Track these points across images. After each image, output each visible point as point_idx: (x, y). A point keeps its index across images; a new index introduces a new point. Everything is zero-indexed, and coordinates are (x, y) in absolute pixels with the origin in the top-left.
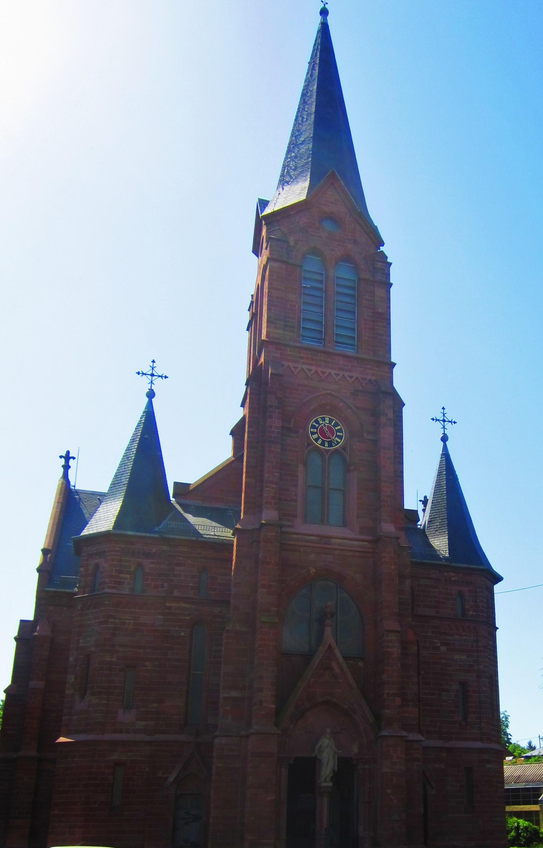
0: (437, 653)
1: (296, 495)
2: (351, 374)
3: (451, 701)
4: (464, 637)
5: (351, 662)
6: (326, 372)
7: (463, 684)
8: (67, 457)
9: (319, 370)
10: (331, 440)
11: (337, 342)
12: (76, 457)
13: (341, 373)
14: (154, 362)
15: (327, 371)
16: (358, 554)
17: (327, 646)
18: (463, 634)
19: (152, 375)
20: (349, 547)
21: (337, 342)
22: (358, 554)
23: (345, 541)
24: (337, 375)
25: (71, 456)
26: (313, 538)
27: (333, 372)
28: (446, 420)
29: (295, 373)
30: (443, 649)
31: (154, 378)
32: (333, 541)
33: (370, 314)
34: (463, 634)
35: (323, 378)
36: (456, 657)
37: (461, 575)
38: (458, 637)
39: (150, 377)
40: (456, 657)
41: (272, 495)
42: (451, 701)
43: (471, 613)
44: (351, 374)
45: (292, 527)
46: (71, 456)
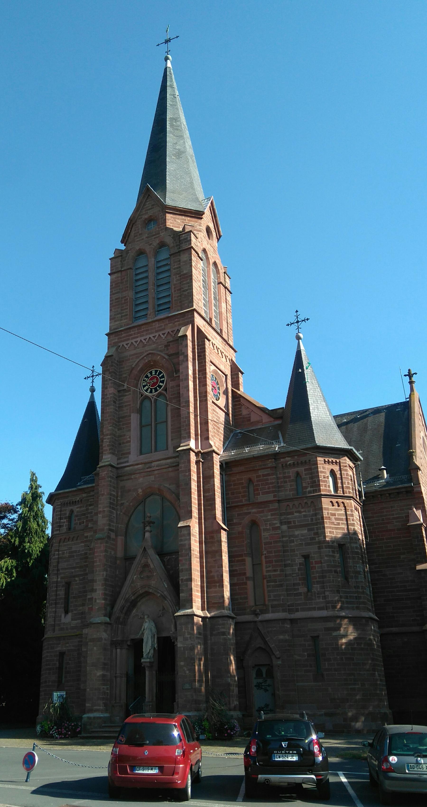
0: (277, 532)
1: (130, 437)
2: (163, 332)
3: (295, 575)
4: (304, 513)
5: (174, 556)
6: (147, 338)
7: (306, 557)
8: (410, 375)
9: (151, 336)
10: (157, 386)
11: (158, 311)
12: (403, 376)
13: (157, 334)
14: (297, 311)
15: (148, 337)
16: (125, 478)
17: (143, 548)
18: (302, 510)
19: (298, 322)
20: (142, 469)
21: (158, 311)
22: (170, 469)
23: (162, 462)
24: (154, 337)
25: (412, 373)
26: (140, 466)
27: (151, 336)
28: (92, 375)
29: (136, 346)
30: (284, 527)
31: (299, 324)
32: (153, 464)
33: (178, 278)
34: (302, 510)
35: (155, 341)
36: (297, 533)
37: (296, 457)
38: (298, 514)
39: (91, 378)
40: (297, 533)
41: (108, 444)
42: (295, 575)
43: (309, 489)
44: (163, 332)
45: (127, 462)
46: (412, 373)
